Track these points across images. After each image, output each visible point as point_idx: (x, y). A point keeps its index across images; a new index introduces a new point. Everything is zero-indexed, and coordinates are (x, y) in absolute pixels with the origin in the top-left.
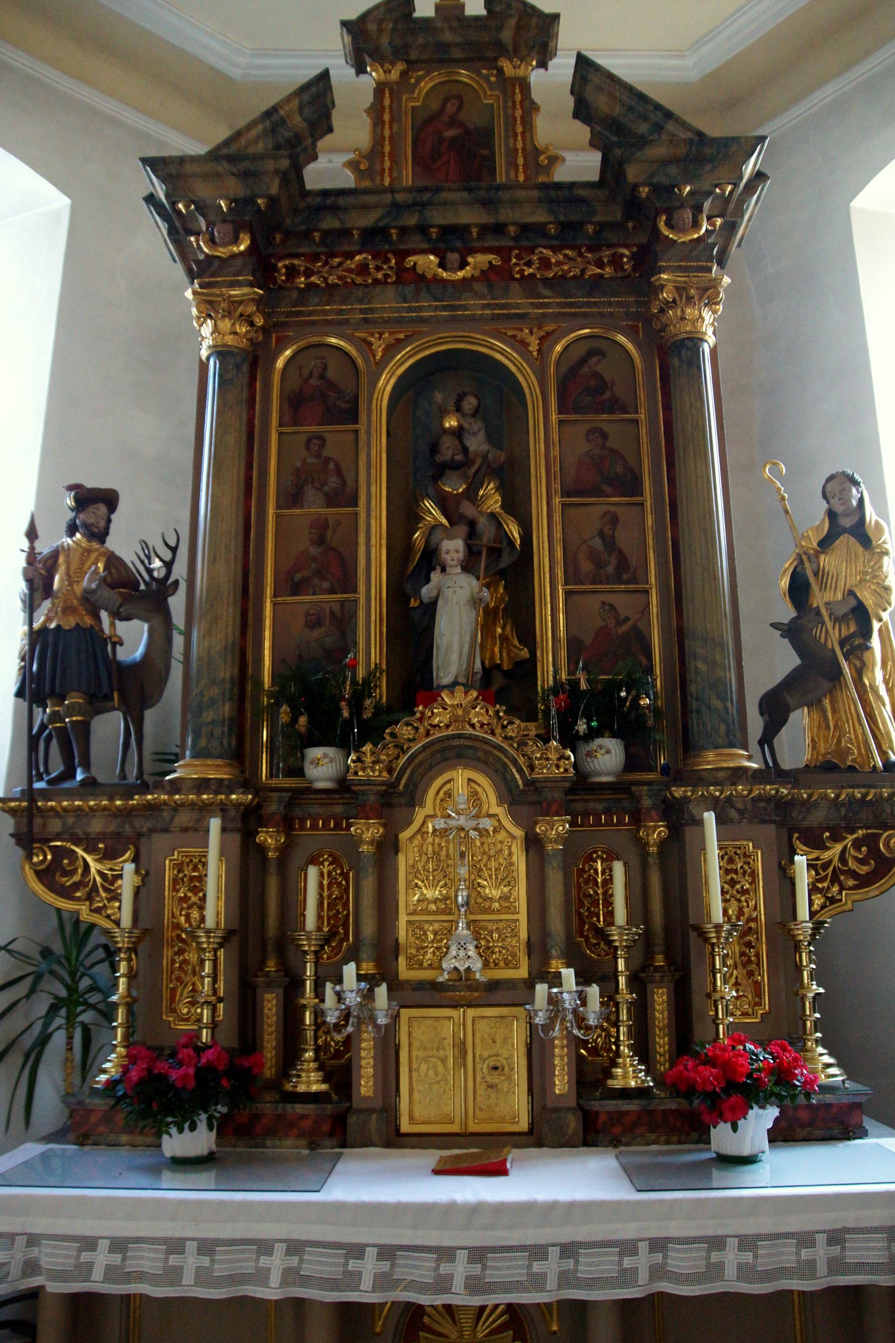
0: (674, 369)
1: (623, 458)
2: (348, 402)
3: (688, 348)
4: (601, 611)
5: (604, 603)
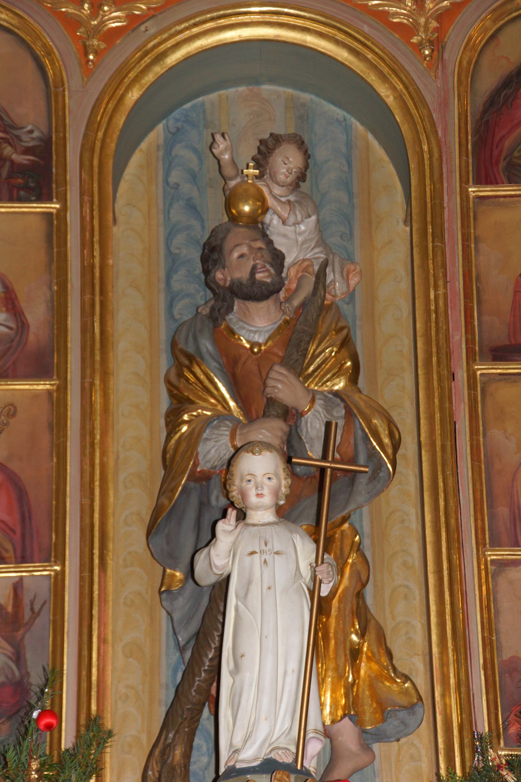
2: (27, 151)
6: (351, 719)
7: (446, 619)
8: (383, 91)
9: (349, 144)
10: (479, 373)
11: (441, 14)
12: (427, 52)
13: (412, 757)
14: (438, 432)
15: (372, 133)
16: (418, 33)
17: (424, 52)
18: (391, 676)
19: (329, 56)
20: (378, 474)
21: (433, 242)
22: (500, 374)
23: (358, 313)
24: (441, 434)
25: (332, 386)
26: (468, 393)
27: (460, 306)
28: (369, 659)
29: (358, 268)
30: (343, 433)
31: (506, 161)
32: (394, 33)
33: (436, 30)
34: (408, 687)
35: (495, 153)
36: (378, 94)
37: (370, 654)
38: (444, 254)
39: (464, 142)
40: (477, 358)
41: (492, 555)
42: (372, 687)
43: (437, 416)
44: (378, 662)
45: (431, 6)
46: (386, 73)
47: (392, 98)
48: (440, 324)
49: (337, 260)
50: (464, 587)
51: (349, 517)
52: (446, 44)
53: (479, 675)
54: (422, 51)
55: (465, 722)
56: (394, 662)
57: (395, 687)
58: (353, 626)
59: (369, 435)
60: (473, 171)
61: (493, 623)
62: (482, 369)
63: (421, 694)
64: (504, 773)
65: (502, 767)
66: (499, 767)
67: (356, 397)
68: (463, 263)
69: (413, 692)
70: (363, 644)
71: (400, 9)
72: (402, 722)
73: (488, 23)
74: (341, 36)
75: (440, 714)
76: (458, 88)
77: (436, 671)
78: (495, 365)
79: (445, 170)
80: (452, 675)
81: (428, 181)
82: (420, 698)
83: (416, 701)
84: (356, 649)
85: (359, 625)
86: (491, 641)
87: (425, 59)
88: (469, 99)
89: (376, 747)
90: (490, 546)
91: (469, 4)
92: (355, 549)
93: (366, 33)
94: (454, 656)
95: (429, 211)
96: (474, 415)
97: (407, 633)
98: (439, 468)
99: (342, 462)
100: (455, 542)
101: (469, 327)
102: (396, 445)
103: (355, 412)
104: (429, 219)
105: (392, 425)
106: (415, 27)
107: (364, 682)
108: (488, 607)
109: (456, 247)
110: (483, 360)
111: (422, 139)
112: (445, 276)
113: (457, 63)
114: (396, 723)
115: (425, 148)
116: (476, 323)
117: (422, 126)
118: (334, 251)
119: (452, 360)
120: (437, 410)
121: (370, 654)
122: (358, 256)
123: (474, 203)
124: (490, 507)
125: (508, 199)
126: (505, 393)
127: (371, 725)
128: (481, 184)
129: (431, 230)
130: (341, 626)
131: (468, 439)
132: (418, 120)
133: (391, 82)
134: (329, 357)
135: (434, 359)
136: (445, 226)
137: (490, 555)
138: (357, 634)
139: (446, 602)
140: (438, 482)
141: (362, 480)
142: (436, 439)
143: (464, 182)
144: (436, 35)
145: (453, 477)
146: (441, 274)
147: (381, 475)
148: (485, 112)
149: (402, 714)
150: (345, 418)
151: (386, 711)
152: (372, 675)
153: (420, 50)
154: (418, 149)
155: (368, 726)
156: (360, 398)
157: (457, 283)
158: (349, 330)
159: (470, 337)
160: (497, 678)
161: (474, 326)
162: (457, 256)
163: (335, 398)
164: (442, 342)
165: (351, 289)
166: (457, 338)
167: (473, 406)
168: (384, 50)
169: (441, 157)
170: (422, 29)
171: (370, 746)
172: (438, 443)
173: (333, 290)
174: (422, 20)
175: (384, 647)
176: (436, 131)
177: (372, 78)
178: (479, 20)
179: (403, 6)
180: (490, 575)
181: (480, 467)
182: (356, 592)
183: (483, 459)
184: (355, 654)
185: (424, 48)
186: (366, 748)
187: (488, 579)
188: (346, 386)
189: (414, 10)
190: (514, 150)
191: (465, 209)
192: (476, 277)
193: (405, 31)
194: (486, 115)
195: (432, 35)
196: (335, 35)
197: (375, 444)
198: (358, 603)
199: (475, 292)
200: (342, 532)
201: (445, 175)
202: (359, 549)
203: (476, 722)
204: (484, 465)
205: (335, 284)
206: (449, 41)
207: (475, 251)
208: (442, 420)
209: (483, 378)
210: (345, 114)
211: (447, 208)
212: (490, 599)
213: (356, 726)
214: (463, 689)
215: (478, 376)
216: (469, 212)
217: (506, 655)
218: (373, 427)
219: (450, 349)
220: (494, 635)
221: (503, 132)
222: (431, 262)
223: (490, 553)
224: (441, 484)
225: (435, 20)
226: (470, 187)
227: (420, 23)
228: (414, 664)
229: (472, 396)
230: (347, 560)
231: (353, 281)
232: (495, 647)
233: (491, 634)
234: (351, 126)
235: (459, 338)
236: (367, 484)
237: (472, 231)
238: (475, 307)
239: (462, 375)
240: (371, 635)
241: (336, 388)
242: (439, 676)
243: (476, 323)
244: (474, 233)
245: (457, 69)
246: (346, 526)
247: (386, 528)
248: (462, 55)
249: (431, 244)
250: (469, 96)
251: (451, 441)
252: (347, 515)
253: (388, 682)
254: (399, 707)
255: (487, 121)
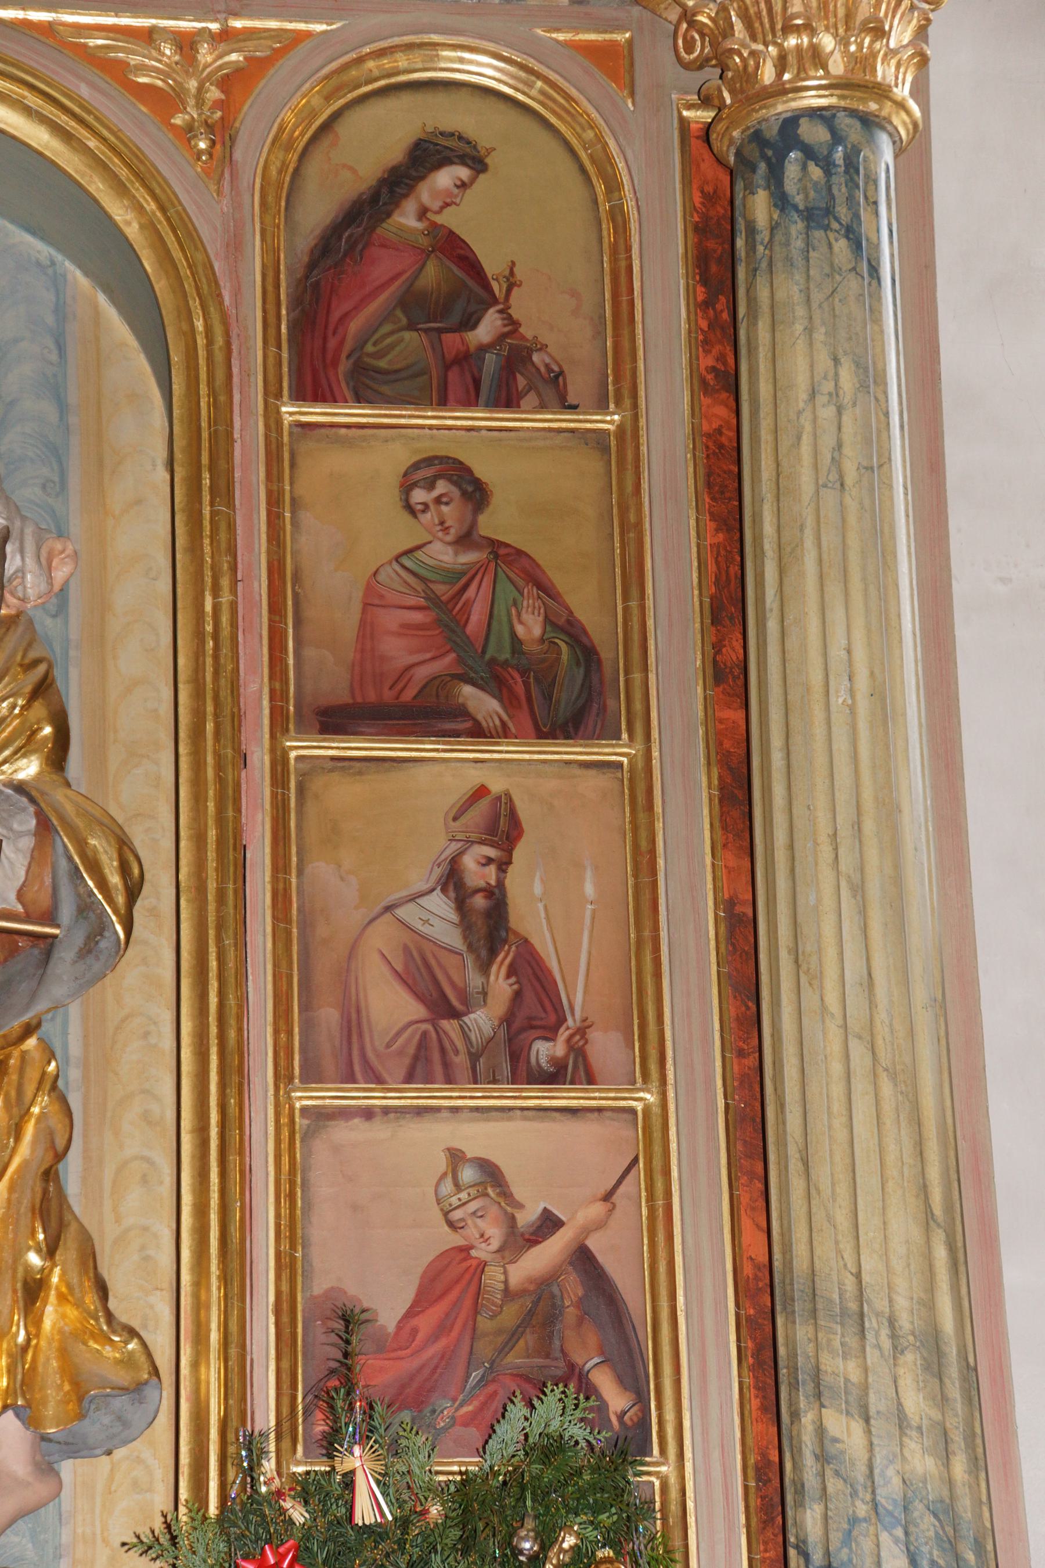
0: (751, 230)
1: (545, 588)
3: (809, 153)
4: (448, 1187)
5: (456, 1157)
6: (17, 1415)
7: (209, 1220)
8: (119, 212)
9: (61, 311)
10: (293, 754)
11: (227, 75)
12: (202, 145)
13: (135, 1484)
14: (212, 864)
15: (104, 292)
16: (185, 108)
17: (196, 145)
18: (102, 1330)
19: (14, 137)
20: (97, 943)
21: (212, 504)
22: (333, 759)
23: (74, 635)
24: (217, 870)
25: (12, 774)
26: (272, 792)
27: (261, 629)
28: (62, 1298)
29: (70, 547)
30: (30, 864)
31: (351, 361)
32: (137, 103)
33: (218, 104)
34: (133, 1349)
35: (332, 343)
36: (109, 217)
37: (64, 1289)
38: (231, 527)
39: (272, 319)
40: (291, 726)
41: (303, 1098)
42: (64, 1353)
43: (212, 834)
44: (79, 1304)
45: (209, 59)
46: (123, 179)
47: (135, 225)
48: (222, 661)
49: (29, 531)
50: (248, 1159)
51: (39, 1025)
52: (238, 132)
53: (265, 1323)
54: (193, 143)
55: (234, 1415)
56: (112, 1304)
57: (108, 1351)
58: (33, 1233)
59: (82, 868)
60: (290, 375)
61: (299, 1225)
62: (302, 747)
63: (158, 1363)
64: (287, 1504)
65: (284, 1494)
66: (279, 1494)
67: (59, 795)
68: (268, 548)
69: (143, 1359)
70: (51, 1270)
71: (150, 59)
72: (119, 1418)
73: (316, 101)
74: (33, 100)
75: (187, 1399)
76: (261, 218)
77: (185, 1318)
78: (324, 740)
79: (235, 370)
80: (214, 1326)
81: (203, 389)
82: (155, 1372)
83: (146, 1376)
84: (35, 1280)
85: (44, 1232)
86: (293, 1259)
87: (199, 159)
88: (282, 239)
89: (67, 1468)
90: (301, 1082)
91: (281, 62)
92: (47, 1086)
93: (84, 100)
94: (219, 1289)
95: (205, 444)
96: (281, 833)
97: (143, 1248)
98: (212, 933)
99: (27, 919)
100: (235, 1073)
101: (278, 669)
102: (133, 892)
103: (55, 823)
104: (205, 459)
105: (125, 848)
106: (179, 96)
107: (49, 1343)
108: (292, 1196)
109: (255, 516)
110: (303, 729)
111: (192, 309)
112: (234, 569)
113: (259, 171)
114: (106, 1420)
115: (199, 325)
116: (291, 661)
117: (193, 284)
118: (23, 513)
119: (243, 729)
120: (211, 822)
121: (64, 1289)
122: (76, 526)
123: (291, 434)
124: (305, 1008)
125: (354, 430)
126: (341, 794)
127: (58, 1426)
128: (304, 400)
129: (208, 481)
130: (11, 1236)
131: (268, 879)
132: (185, 272)
133: (134, 197)
134: (8, 717)
135: (210, 727)
136: (236, 475)
137: (301, 1098)
138: (39, 1251)
139: (212, 1188)
140: (208, 959)
141: (65, 956)
142: (207, 878)
143: (272, 393)
144: (219, 114)
145: (236, 950)
146: (226, 566)
147: (103, 944)
148: (312, 266)
149: (120, 1403)
150: (35, 835)
151: (87, 1397)
152: (66, 1328)
153: (189, 140)
154: (185, 327)
155: (50, 1428)
156: (66, 796)
157: (256, 584)
158: (50, 666)
159: (277, 686)
160: (300, 1330)
161: (287, 665)
162: (256, 536)
163: (18, 796)
164: (225, 694)
165: (57, 588)
166: (253, 687)
167: (281, 815)
168: (119, 134)
169: (228, 344)
170: (192, 102)
171: (55, 1466)
172: (212, 886)
173: (20, 588)
174: (193, 84)
175: (92, 1275)
176: (220, 295)
177: (98, 187)
178: (299, 94)
179: (154, 53)
180: (298, 1136)
181: (289, 933)
182: (42, 1170)
183: (295, 918)
184: (33, 1290)
185: (195, 136)
186: (46, 1469)
187: (295, 1144)
188: (40, 774)
189: (177, 63)
190: (365, 342)
191: (274, 446)
192: (292, 574)
193: (162, 101)
194: (315, 272)
195: (212, 113)
196: (24, 97)
197: (91, 883)
198: (45, 1192)
199: (290, 603)
200: (24, 1054)
201: (236, 380)
202: (54, 1087)
203: (253, 1413)
204: (298, 928)
205: (23, 577)
206: (242, 128)
207: (292, 524)
208: (221, 841)
209: (301, 766)
210: (53, 252)
211: (239, 441)
212: (295, 1182)
213: (28, 1429)
214: (233, 1351)
215: (292, 762)
216: (281, 453)
217: (319, 1287)
218: (90, 853)
219: (240, 710)
220: (300, 1248)
221: (346, 306)
222: (207, 541)
223: (299, 1094)
224: (213, 964)
225: (217, 86)
226: (284, 404)
227: (188, 90)
228: (152, 1307)
229: (279, 797)
230: (29, 1109)
231: (60, 574)
232: (300, 1271)
233: (293, 1247)
234: (64, 276)
235: (256, 688)
236: (75, 962)
237: (287, 488)
238: (290, 631)
239: (260, 758)
240: (68, 1252)
241: (21, 776)
242: (190, 1327)
243: (291, 661)
244: (291, 492)
245: (258, 181)
246: (31, 1042)
247: (112, 1049)
248: (268, 155)
249: (208, 508)
250: (282, 234)
251: (235, 883)
252: (34, 1022)
253: (96, 1342)
254: (112, 1388)
255: (317, 284)
